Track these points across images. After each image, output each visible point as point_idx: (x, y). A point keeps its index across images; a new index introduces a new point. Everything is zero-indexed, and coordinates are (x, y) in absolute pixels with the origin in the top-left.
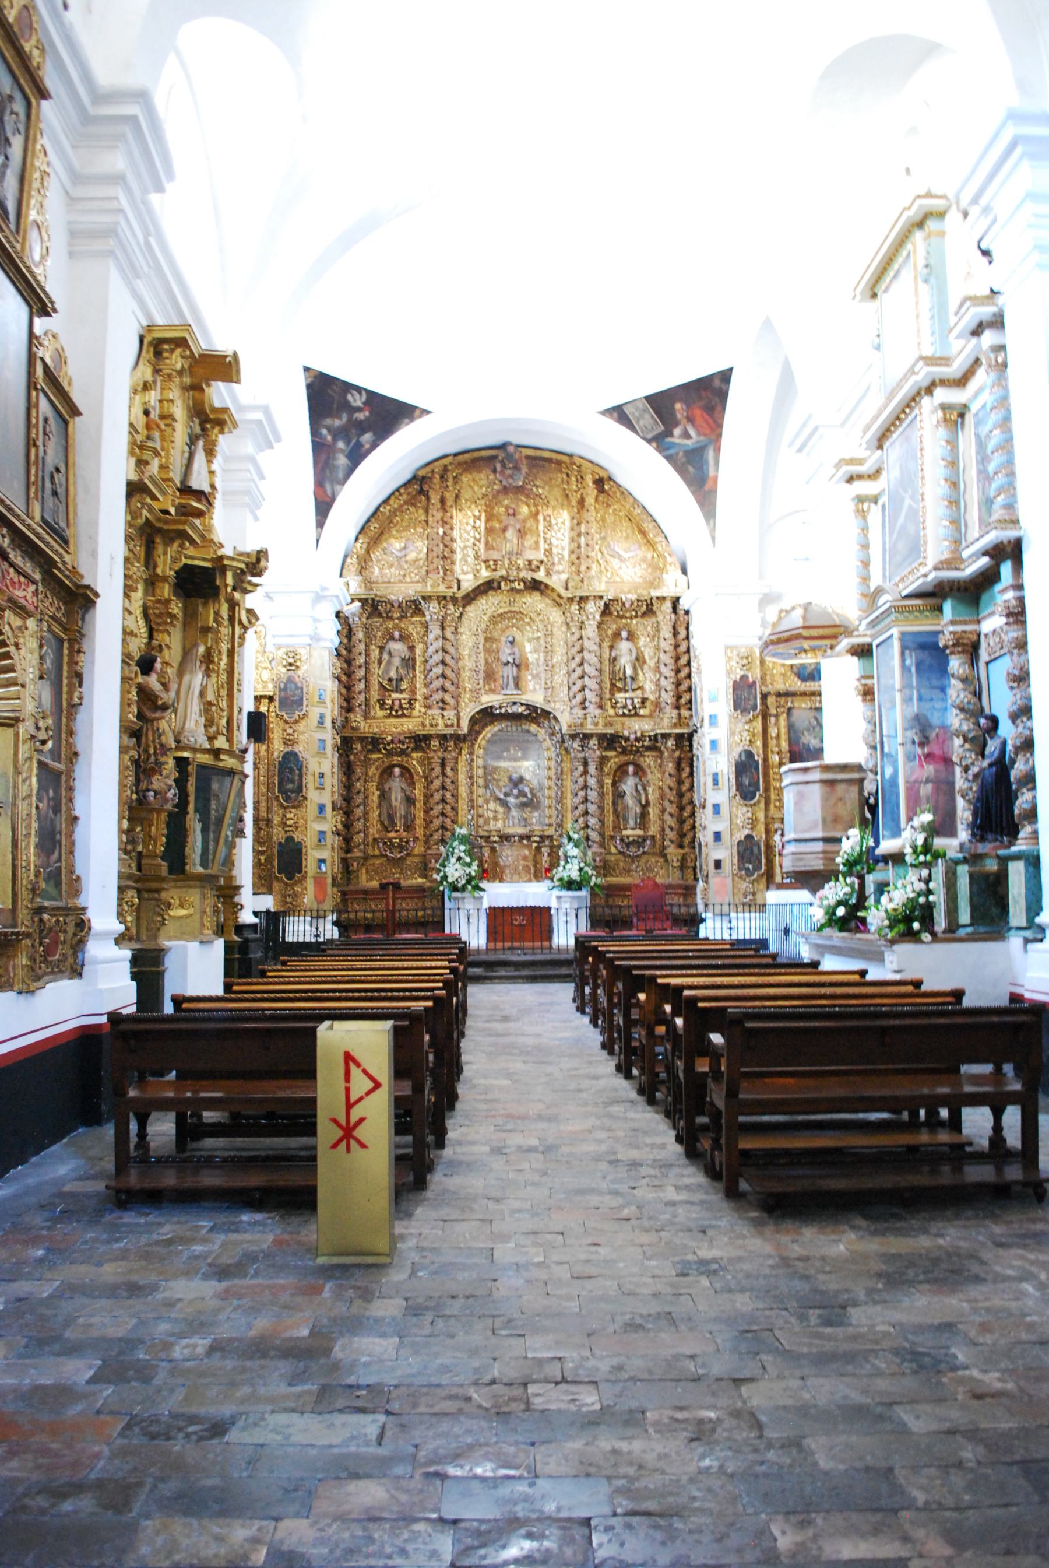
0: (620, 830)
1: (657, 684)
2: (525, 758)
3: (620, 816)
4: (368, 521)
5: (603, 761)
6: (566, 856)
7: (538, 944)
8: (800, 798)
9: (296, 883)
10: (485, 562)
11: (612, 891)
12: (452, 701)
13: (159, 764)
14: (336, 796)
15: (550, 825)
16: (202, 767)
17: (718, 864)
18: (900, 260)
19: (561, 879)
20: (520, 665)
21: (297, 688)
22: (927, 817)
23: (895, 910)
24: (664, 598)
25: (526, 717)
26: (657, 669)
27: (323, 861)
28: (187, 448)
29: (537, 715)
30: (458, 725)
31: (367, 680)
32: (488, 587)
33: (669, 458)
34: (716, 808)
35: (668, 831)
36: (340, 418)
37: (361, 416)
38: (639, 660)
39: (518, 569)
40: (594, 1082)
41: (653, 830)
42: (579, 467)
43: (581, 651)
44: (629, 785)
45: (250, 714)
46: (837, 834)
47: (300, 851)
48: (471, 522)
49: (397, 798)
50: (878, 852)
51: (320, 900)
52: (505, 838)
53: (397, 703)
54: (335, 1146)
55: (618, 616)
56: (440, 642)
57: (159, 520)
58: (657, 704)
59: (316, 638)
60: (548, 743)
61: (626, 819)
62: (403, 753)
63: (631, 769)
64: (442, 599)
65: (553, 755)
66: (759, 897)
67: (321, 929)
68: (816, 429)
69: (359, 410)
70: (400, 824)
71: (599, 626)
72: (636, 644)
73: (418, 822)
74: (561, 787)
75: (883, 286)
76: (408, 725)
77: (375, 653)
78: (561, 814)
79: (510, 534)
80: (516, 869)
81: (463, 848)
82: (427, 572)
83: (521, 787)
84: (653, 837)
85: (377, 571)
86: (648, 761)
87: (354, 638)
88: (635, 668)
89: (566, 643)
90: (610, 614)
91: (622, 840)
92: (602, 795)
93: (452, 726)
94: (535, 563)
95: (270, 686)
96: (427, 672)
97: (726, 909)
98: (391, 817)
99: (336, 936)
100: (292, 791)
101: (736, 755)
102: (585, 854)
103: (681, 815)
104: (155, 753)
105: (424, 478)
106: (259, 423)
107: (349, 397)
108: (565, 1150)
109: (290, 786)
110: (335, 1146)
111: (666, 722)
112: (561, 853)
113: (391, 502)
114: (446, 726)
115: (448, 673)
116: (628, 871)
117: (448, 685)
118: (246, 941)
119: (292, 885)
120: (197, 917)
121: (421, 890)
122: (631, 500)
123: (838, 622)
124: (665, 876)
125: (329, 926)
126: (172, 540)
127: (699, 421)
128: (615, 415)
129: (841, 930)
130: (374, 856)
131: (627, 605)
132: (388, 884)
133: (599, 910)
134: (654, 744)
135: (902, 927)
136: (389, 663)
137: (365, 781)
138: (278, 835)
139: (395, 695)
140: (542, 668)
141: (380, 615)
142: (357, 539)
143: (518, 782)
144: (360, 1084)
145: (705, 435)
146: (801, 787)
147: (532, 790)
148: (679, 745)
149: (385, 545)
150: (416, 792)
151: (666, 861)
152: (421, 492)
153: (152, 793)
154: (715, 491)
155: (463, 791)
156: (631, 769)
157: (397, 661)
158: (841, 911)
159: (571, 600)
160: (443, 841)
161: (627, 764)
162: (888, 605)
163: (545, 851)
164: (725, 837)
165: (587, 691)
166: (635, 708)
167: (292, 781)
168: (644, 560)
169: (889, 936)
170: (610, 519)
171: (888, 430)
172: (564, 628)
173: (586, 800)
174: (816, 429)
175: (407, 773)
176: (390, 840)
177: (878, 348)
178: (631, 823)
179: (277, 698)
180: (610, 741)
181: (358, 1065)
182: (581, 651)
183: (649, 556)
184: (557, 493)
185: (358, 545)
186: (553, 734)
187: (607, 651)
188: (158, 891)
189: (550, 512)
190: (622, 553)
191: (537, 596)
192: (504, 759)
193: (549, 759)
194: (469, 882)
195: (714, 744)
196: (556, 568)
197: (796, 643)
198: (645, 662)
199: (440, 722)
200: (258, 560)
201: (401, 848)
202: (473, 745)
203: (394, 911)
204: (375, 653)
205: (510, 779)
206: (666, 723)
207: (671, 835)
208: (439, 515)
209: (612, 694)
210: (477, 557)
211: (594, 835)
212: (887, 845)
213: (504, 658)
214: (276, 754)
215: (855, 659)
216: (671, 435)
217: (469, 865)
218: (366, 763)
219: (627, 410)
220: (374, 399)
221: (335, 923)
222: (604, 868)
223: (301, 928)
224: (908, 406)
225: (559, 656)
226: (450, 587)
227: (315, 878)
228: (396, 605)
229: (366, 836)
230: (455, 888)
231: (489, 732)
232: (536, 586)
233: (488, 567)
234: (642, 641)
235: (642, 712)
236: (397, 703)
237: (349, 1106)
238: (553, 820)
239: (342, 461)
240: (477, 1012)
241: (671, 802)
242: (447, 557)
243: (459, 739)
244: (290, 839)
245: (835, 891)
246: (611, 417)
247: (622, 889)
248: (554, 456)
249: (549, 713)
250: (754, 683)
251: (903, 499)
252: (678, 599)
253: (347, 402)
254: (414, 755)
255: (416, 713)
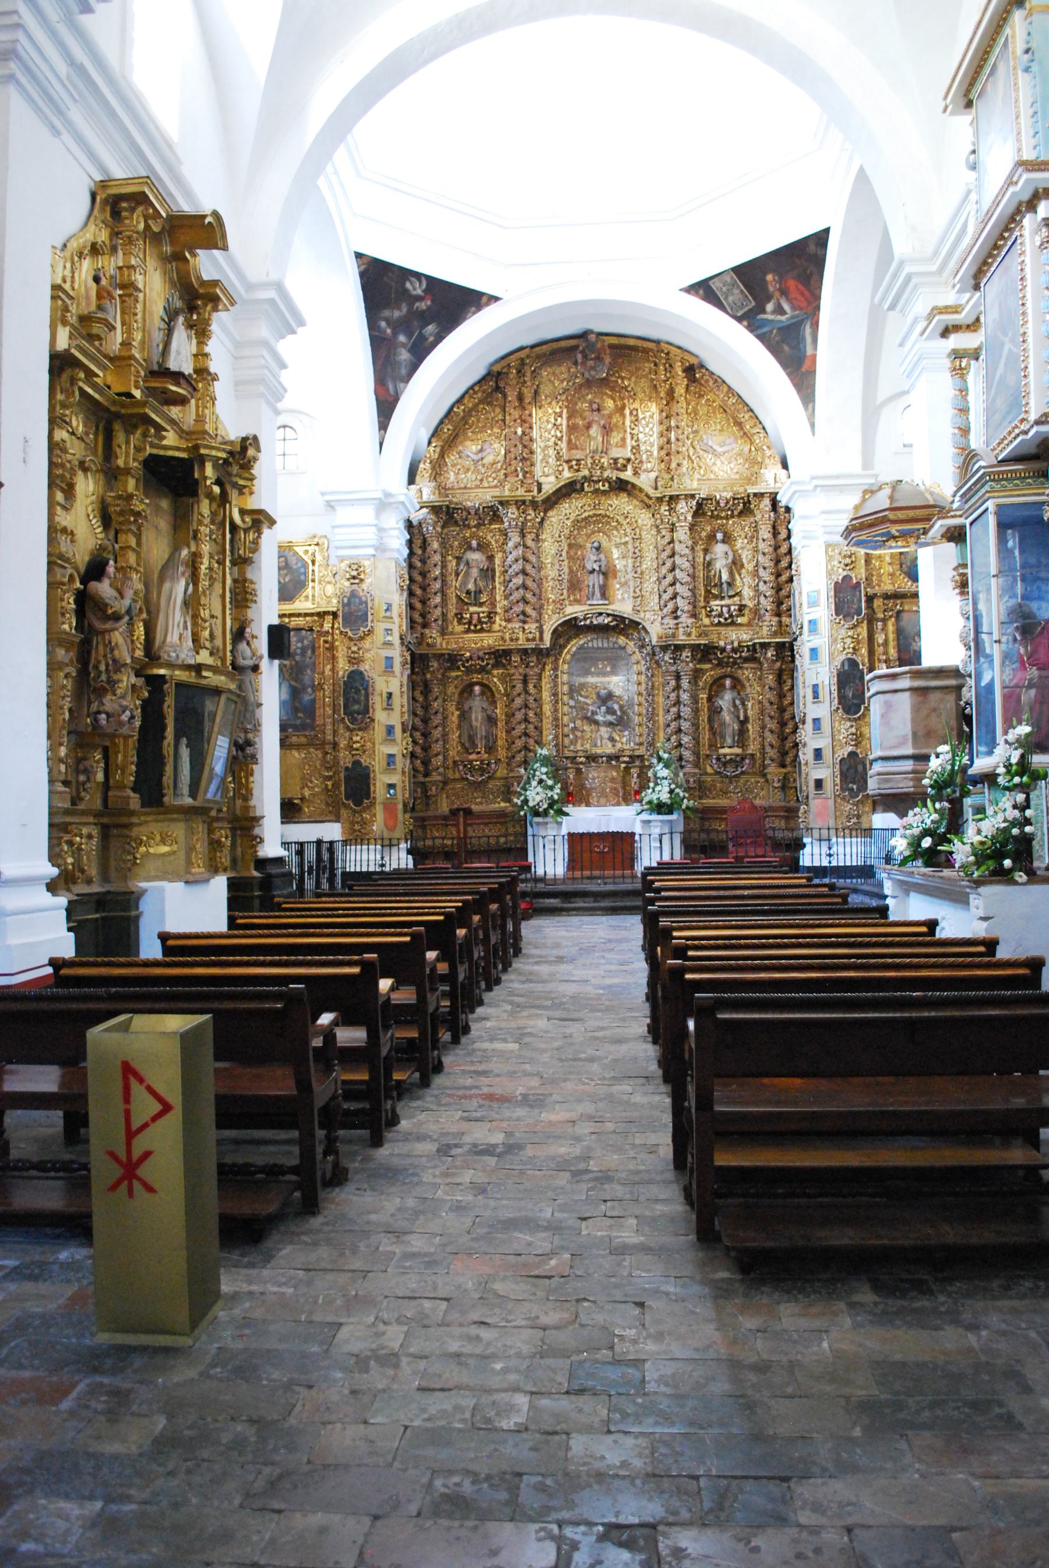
0: (717, 749)
1: (756, 589)
2: (614, 672)
3: (716, 734)
4: (441, 422)
5: (697, 674)
6: (656, 778)
7: (618, 873)
8: (888, 706)
9: (364, 810)
10: (568, 462)
11: (705, 814)
12: (533, 614)
13: (112, 683)
14: (406, 717)
15: (641, 744)
16: (180, 685)
17: (819, 784)
18: (997, 50)
19: (650, 802)
20: (607, 573)
21: (361, 602)
22: (1024, 729)
23: (982, 843)
24: (762, 495)
25: (614, 628)
26: (755, 574)
27: (391, 786)
28: (163, 325)
29: (625, 626)
30: (541, 639)
31: (444, 595)
32: (569, 490)
33: (761, 338)
34: (816, 721)
35: (768, 749)
36: (399, 309)
37: (422, 306)
38: (736, 564)
39: (602, 467)
40: (613, 1048)
41: (753, 748)
42: (668, 354)
43: (673, 555)
44: (725, 700)
45: (271, 628)
46: (924, 751)
47: (368, 776)
48: (553, 420)
49: (477, 718)
50: (970, 772)
51: (391, 828)
52: (592, 758)
53: (475, 616)
54: (114, 1188)
55: (712, 517)
56: (520, 551)
57: (114, 402)
58: (756, 612)
59: (381, 548)
60: (638, 656)
61: (723, 737)
62: (483, 670)
63: (728, 682)
64: (520, 503)
65: (644, 669)
66: (864, 819)
67: (387, 859)
68: (908, 278)
69: (419, 298)
70: (481, 746)
71: (692, 528)
72: (732, 546)
73: (500, 743)
74: (652, 704)
75: (978, 87)
76: (488, 640)
77: (452, 564)
78: (653, 732)
79: (594, 431)
80: (603, 790)
81: (544, 770)
82: (506, 475)
83: (609, 704)
84: (752, 755)
85: (452, 476)
86: (747, 673)
87: (429, 549)
88: (731, 574)
89: (656, 547)
90: (704, 514)
91: (718, 759)
92: (696, 711)
93: (534, 639)
94: (621, 461)
95: (335, 601)
96: (506, 583)
97: (825, 833)
98: (472, 739)
99: (411, 866)
100: (358, 713)
101: (838, 663)
102: (676, 775)
103: (782, 732)
104: (107, 670)
105: (499, 373)
106: (272, 302)
107: (408, 285)
108: (529, 1151)
109: (356, 707)
110: (114, 1188)
111: (765, 631)
112: (650, 774)
113: (466, 401)
114: (528, 640)
115: (529, 583)
116: (725, 793)
117: (529, 596)
118: (270, 876)
119: (359, 812)
120: (182, 854)
121: (502, 815)
122: (725, 389)
123: (931, 502)
124: (765, 797)
125: (403, 854)
126: (135, 427)
127: (794, 294)
128: (701, 292)
129: (927, 864)
130: (455, 780)
131: (722, 505)
132: (458, 810)
133: (695, 835)
134: (753, 653)
135: (991, 864)
136: (467, 574)
137: (444, 701)
138: (345, 759)
139: (473, 609)
140: (630, 576)
141: (456, 523)
142: (430, 443)
143: (607, 698)
144: (144, 1106)
145: (801, 309)
146: (888, 696)
147: (621, 707)
148: (779, 656)
149: (460, 448)
150: (498, 711)
151: (767, 781)
152: (497, 389)
153: (104, 716)
154: (815, 371)
155: (547, 709)
156: (728, 682)
157: (475, 572)
158: (927, 842)
159: (660, 500)
160: (525, 763)
161: (724, 677)
162: (982, 472)
163: (634, 772)
164: (827, 754)
165: (679, 599)
166: (731, 616)
167: (358, 702)
168: (740, 454)
169: (976, 874)
170: (702, 411)
171: (985, 263)
172: (654, 532)
173: (678, 717)
174: (908, 278)
175: (487, 690)
176: (471, 762)
177: (973, 167)
178: (729, 741)
179: (340, 614)
180: (705, 652)
181: (141, 1080)
182: (673, 555)
183: (746, 449)
184: (644, 383)
185: (432, 449)
186: (643, 647)
187: (701, 554)
188: (128, 826)
189: (636, 405)
190: (716, 447)
191: (624, 498)
192: (592, 674)
193: (639, 673)
194: (551, 806)
195: (814, 651)
196: (644, 466)
197: (881, 529)
198: (742, 566)
199: (521, 635)
200: (244, 449)
201: (482, 770)
202: (557, 660)
203: (465, 837)
204: (452, 564)
205: (598, 695)
206: (765, 632)
207: (771, 753)
208: (516, 414)
209: (707, 600)
210: (558, 457)
211: (687, 754)
212: (982, 764)
213: (589, 566)
214: (341, 673)
215: (952, 545)
216: (764, 312)
217: (551, 788)
218: (444, 682)
219: (715, 285)
220: (435, 285)
221: (409, 852)
222: (698, 789)
223: (365, 857)
224: (1007, 229)
225: (649, 562)
226: (530, 491)
227: (384, 804)
228: (473, 512)
229: (445, 758)
230: (536, 813)
231: (573, 646)
232: (622, 486)
233: (571, 467)
234: (739, 543)
235: (740, 620)
236: (475, 616)
237: (131, 1135)
238: (643, 739)
239: (404, 355)
240: (534, 951)
241: (772, 718)
242: (527, 459)
243: (541, 654)
244: (357, 763)
245: (923, 817)
246: (697, 294)
247: (718, 812)
248: (639, 343)
249: (639, 624)
250: (858, 584)
251: (1003, 345)
252: (777, 494)
253: (407, 291)
254: (495, 672)
255: (496, 627)
